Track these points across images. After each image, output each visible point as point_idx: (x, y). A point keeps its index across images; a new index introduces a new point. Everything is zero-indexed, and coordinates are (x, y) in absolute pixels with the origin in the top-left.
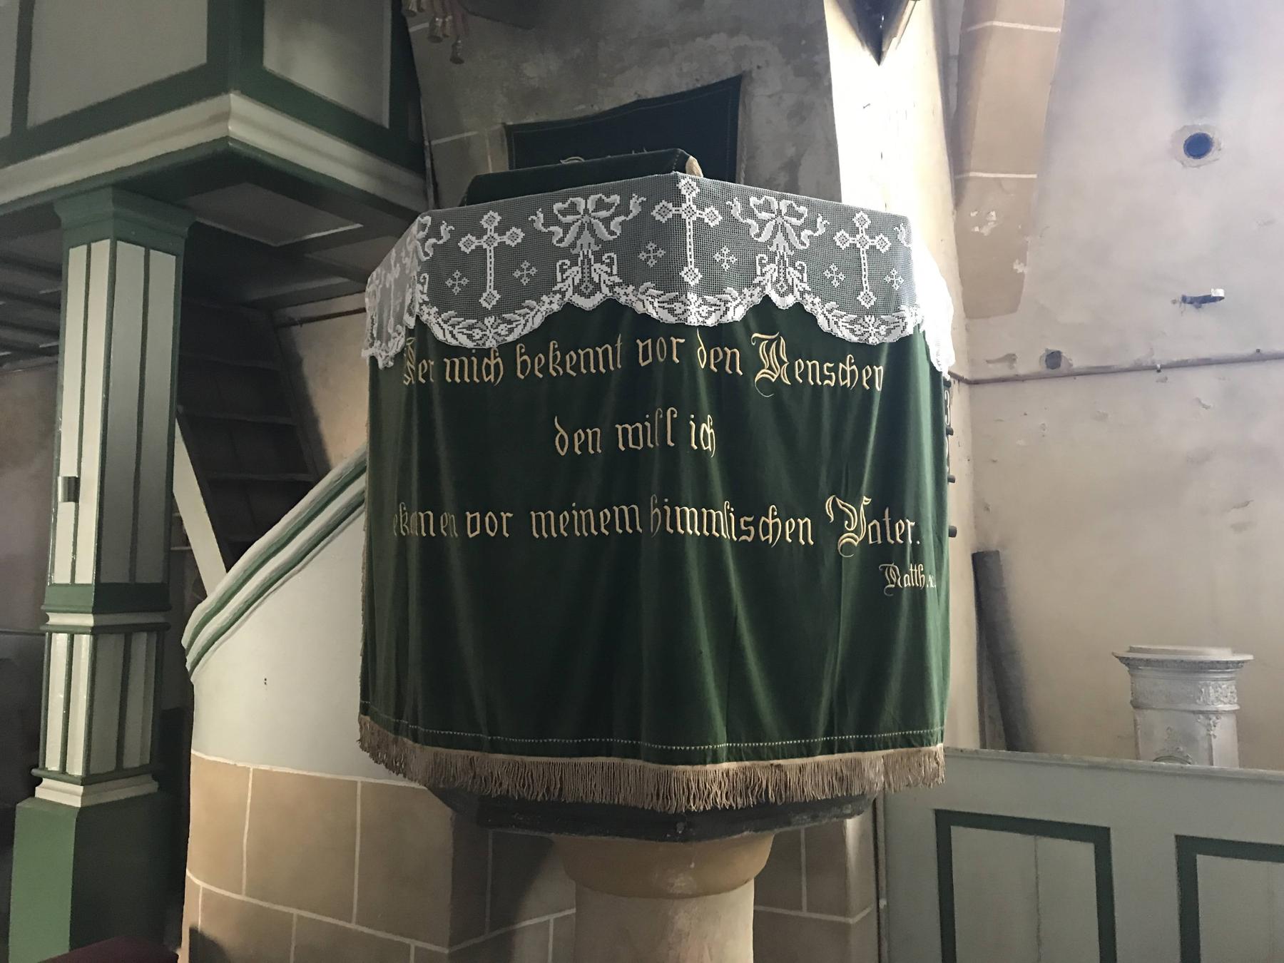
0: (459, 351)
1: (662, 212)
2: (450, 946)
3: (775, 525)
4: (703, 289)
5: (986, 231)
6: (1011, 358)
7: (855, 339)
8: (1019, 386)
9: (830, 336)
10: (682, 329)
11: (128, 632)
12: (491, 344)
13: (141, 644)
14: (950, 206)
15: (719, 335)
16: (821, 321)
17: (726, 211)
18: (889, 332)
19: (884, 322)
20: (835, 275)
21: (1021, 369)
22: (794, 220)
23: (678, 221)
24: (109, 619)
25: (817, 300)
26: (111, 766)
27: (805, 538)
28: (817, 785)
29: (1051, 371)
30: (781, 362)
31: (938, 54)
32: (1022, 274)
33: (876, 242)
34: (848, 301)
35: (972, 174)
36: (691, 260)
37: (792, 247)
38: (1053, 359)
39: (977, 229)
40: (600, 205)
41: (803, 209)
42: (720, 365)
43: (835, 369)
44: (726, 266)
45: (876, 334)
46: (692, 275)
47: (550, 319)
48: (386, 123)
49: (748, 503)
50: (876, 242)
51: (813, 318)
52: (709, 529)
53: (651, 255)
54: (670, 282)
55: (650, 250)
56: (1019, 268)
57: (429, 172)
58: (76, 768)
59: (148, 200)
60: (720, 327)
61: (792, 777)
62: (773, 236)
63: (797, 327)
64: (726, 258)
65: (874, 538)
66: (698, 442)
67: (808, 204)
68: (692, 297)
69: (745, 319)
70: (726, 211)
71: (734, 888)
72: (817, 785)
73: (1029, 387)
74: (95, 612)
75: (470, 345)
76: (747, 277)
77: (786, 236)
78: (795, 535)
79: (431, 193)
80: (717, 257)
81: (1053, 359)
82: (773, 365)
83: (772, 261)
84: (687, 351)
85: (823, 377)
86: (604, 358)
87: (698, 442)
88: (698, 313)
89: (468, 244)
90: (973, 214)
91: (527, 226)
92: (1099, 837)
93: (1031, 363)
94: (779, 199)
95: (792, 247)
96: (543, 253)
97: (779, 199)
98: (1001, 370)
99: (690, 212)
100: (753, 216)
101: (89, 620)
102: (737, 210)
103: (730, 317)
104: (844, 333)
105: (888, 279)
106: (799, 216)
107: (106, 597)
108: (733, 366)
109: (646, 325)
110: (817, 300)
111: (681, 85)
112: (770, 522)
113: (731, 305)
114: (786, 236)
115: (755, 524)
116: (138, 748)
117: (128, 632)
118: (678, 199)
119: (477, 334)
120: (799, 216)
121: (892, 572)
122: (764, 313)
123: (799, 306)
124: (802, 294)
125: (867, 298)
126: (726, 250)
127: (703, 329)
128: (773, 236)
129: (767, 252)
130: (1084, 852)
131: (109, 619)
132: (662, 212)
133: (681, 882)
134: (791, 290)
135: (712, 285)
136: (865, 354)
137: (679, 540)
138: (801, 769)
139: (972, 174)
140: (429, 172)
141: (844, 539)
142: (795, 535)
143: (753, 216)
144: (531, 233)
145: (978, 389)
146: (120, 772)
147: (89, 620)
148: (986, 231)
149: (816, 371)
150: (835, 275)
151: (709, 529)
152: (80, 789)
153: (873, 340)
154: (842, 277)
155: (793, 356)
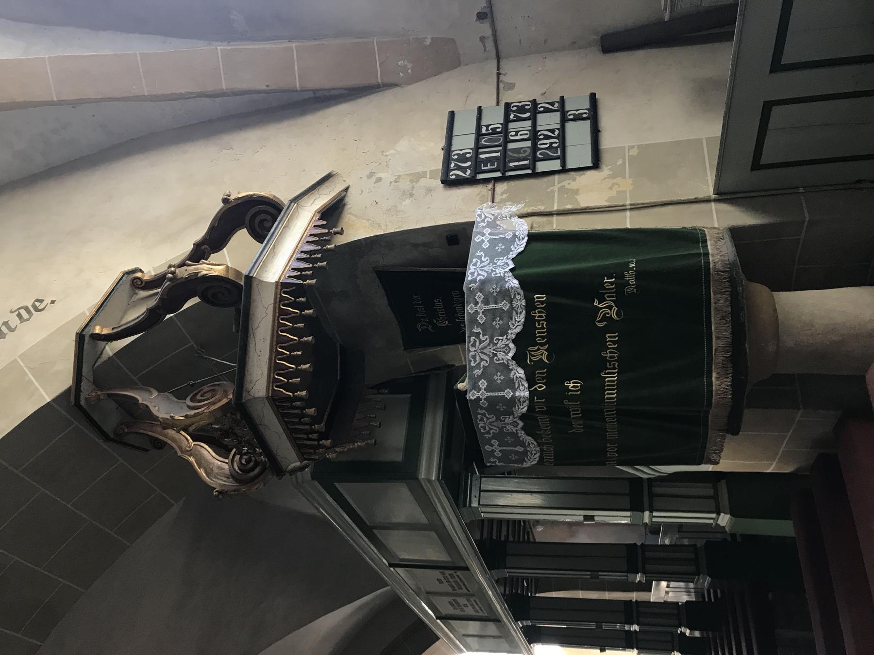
0: (541, 457)
1: (484, 404)
2: (799, 409)
3: (610, 352)
4: (514, 390)
5: (410, 66)
6: (482, 39)
7: (524, 312)
8: (498, 33)
9: (525, 325)
10: (531, 399)
11: (651, 495)
12: (538, 449)
13: (658, 490)
14: (397, 90)
15: (531, 380)
16: (518, 330)
17: (480, 378)
18: (519, 294)
19: (515, 296)
20: (498, 323)
21: (488, 32)
22: (477, 344)
23: (487, 399)
24: (646, 504)
25: (509, 332)
26: (712, 500)
27: (615, 337)
28: (725, 330)
29: (489, 15)
30: (539, 349)
31: (318, 109)
32: (432, 39)
33: (480, 301)
34: (508, 315)
35: (380, 81)
36: (502, 394)
37: (489, 345)
38: (481, 16)
39: (410, 71)
40: (482, 420)
41: (472, 339)
42: (543, 378)
43: (539, 321)
44: (502, 378)
45: (520, 302)
46: (508, 394)
47: (528, 434)
48: (409, 396)
49: (603, 364)
50: (480, 301)
51: (518, 334)
52: (613, 386)
53: (501, 407)
54: (514, 401)
55: (500, 407)
56: (428, 41)
57: (428, 373)
58: (714, 516)
59: (457, 491)
60: (528, 380)
61: (721, 344)
62: (485, 354)
63: (523, 341)
64: (499, 378)
65: (613, 297)
66: (577, 391)
67: (469, 337)
68: (517, 394)
69: (523, 368)
70: (480, 378)
71: (775, 310)
72: (725, 330)
73: (499, 26)
74: (643, 511)
75: (538, 454)
76: (504, 368)
77: (486, 347)
78: (614, 342)
79: (436, 372)
80: (499, 381)
81: (481, 16)
82: (542, 354)
83: (496, 355)
84: (540, 395)
85: (543, 328)
86: (544, 421)
87: (577, 391)
88: (523, 393)
89: (498, 454)
90: (402, 75)
91: (490, 439)
92: (768, 107)
93: (485, 28)
94: (470, 351)
95: (489, 345)
96: (501, 436)
97: (470, 351)
98: (490, 44)
99: (483, 394)
100: (479, 364)
101: (647, 513)
102: (478, 372)
103: (523, 376)
104: (521, 318)
105: (495, 294)
106: (475, 341)
107: (636, 507)
108: (543, 373)
109: (531, 408)
110: (509, 332)
111: (381, 291)
112: (609, 355)
113: (518, 375)
114: (486, 347)
115: (610, 362)
116: (706, 490)
117: (651, 495)
118: (478, 399)
119: (534, 452)
120: (475, 341)
121: (628, 290)
122: (519, 359)
123: (514, 341)
124: (508, 340)
125: (504, 306)
126: (496, 378)
127: (530, 387)
128: (485, 354)
129: (493, 357)
130: (776, 111)
131: (646, 504)
132: (484, 404)
133: (771, 348)
134: (507, 345)
135: (510, 384)
136: (530, 306)
137: (619, 401)
138: (717, 338)
139: (380, 81)
140: (428, 373)
141: (615, 317)
142: (614, 342)
143: (479, 364)
144: (494, 437)
145: (502, 54)
146: (715, 497)
147: (647, 513)
148: (410, 66)
149: (541, 328)
150: (498, 323)
151: (613, 386)
152: (722, 514)
153: (524, 303)
154: (498, 319)
155: (536, 344)
